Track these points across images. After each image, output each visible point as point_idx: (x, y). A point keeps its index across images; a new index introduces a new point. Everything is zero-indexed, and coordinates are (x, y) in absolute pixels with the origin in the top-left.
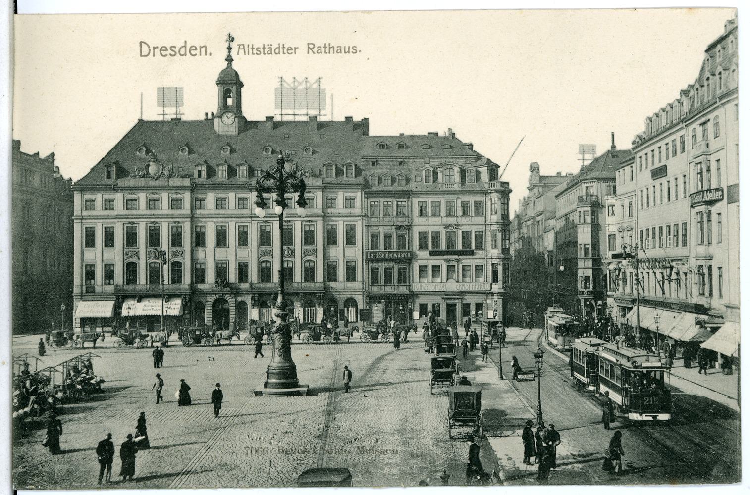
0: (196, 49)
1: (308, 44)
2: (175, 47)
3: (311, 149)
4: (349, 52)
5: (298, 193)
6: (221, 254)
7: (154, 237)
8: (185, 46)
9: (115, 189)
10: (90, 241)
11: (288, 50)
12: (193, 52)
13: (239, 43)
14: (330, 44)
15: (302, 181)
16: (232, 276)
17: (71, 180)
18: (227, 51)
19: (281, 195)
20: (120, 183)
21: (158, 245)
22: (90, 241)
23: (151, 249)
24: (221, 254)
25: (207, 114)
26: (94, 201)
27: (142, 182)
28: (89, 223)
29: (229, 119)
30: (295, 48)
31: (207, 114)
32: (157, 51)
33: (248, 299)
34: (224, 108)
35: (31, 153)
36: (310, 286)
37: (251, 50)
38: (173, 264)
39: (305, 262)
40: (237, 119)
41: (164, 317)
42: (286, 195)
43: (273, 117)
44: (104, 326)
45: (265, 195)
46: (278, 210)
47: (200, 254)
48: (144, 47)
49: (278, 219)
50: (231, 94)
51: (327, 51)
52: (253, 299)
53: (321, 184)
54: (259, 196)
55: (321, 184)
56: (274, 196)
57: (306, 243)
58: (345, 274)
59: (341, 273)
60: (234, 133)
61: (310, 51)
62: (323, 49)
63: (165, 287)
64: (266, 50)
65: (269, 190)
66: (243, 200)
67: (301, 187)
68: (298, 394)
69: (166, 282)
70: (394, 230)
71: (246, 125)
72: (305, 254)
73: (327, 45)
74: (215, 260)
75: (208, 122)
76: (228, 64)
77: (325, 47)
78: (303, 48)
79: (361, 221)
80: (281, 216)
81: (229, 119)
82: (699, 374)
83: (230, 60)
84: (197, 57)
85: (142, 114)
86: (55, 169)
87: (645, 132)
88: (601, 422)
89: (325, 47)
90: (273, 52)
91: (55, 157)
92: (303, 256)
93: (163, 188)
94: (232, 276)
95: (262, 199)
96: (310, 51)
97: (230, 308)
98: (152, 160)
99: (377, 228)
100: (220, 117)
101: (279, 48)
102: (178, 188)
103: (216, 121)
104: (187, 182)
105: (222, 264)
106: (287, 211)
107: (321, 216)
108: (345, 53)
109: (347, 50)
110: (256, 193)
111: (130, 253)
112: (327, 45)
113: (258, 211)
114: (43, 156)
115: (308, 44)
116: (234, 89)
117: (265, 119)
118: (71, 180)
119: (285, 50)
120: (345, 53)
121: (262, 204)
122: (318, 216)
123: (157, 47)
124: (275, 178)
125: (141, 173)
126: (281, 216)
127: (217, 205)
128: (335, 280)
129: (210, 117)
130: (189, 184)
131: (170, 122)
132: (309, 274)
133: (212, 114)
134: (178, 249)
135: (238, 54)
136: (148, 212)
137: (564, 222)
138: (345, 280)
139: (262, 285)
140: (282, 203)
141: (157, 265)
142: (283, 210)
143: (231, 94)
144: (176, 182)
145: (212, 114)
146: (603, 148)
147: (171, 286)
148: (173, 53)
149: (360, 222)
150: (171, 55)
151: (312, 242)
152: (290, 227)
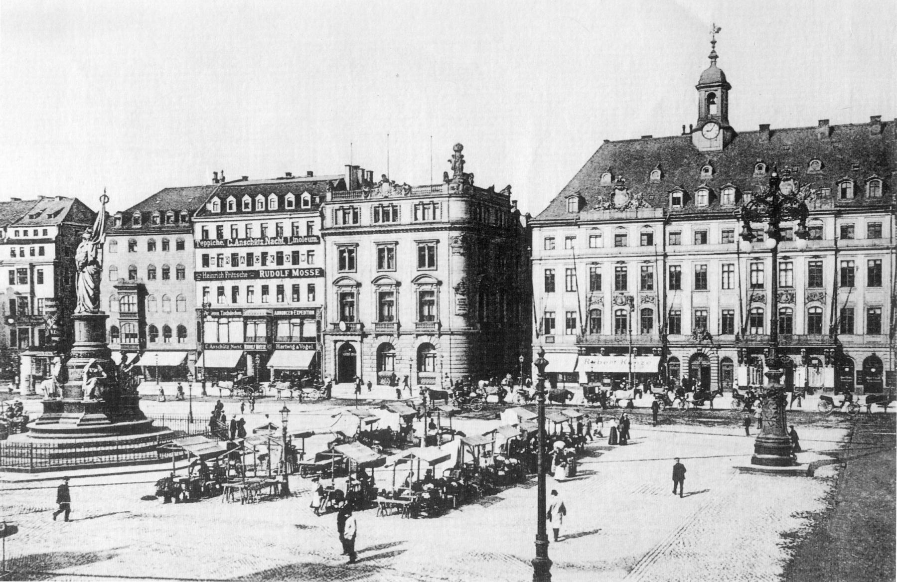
5: (798, 221)
7: (621, 282)
9: (576, 223)
10: (550, 286)
15: (803, 206)
18: (711, 45)
19: (774, 223)
20: (584, 216)
21: (626, 289)
22: (550, 286)
23: (617, 293)
24: (700, 298)
25: (684, 127)
26: (680, 234)
27: (607, 215)
28: (550, 265)
29: (712, 130)
31: (684, 127)
33: (733, 354)
34: (705, 119)
35: (486, 187)
36: (815, 340)
38: (643, 311)
39: (809, 309)
40: (721, 130)
41: (632, 374)
42: (782, 225)
43: (769, 125)
44: (566, 381)
45: (754, 225)
46: (770, 243)
49: (771, 254)
50: (715, 100)
52: (740, 354)
53: (833, 208)
54: (747, 226)
55: (833, 208)
56: (765, 225)
57: (811, 284)
59: (860, 323)
60: (718, 149)
63: (634, 338)
65: (758, 218)
66: (728, 232)
67: (801, 213)
68: (794, 473)
69: (634, 333)
71: (731, 136)
72: (810, 298)
75: (687, 137)
76: (712, 62)
80: (774, 251)
81: (712, 130)
82: (673, 494)
83: (714, 57)
86: (511, 204)
91: (512, 190)
93: (630, 221)
95: (750, 229)
97: (712, 365)
98: (619, 187)
100: (700, 129)
102: (647, 221)
103: (696, 136)
104: (659, 213)
105: (729, 311)
106: (782, 245)
110: (742, 223)
113: (745, 246)
114: (497, 190)
116: (718, 93)
117: (758, 128)
121: (749, 236)
124: (766, 203)
125: (606, 205)
126: (774, 251)
127: (696, 240)
128: (850, 331)
129: (688, 130)
130: (661, 216)
131: (640, 140)
132: (814, 322)
133: (691, 126)
134: (817, 290)
136: (870, 242)
139: (811, 337)
140: (776, 234)
141: (624, 313)
142: (778, 243)
143: (715, 100)
144: (646, 213)
145: (691, 126)
151: (820, 285)
152: (819, 264)
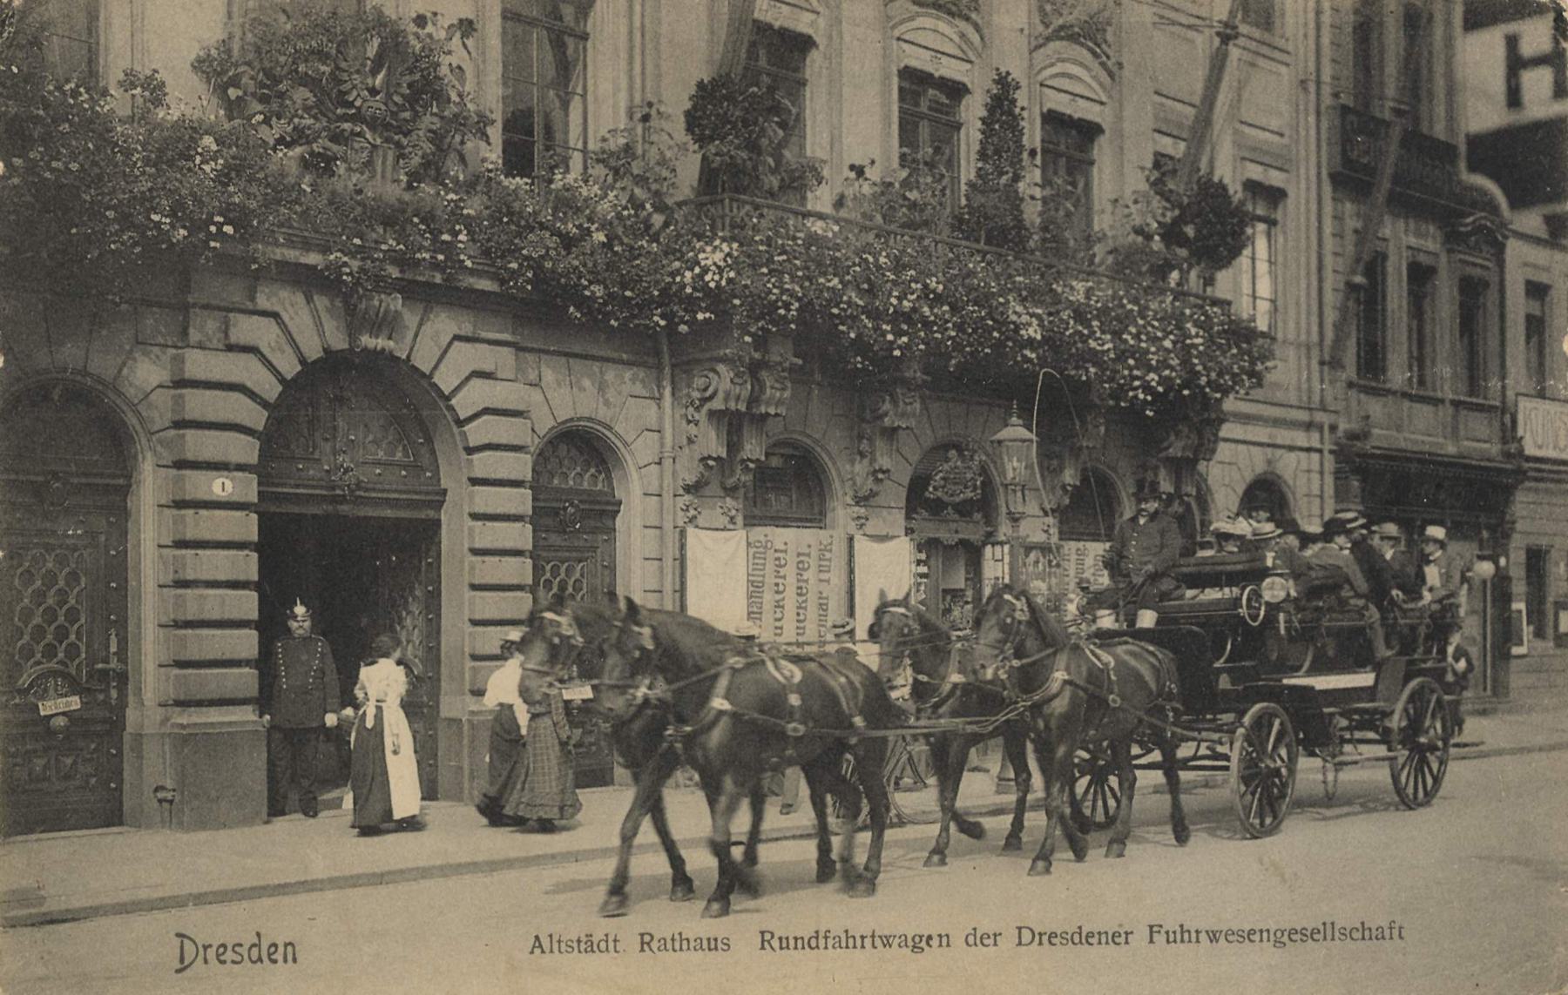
0: (1319, 932)
1: (642, 935)
2: (241, 945)
4: (716, 948)
8: (1080, 934)
11: (1087, 936)
12: (986, 942)
13: (643, 931)
14: (680, 934)
17: (1080, 855)
30: (995, 935)
32: (1045, 938)
37: (556, 946)
51: (677, 946)
61: (646, 947)
64: (583, 946)
85: (436, 367)
87: (340, 400)
88: (809, 836)
90: (595, 948)
96: (646, 947)
101: (817, 938)
108: (710, 949)
109: (1265, 934)
112: (677, 937)
115: (642, 935)
118: (1080, 855)
119: (563, 945)
120: (1268, 931)
123: (210, 946)
137: (937, 832)
148: (238, 958)
150: (234, 962)
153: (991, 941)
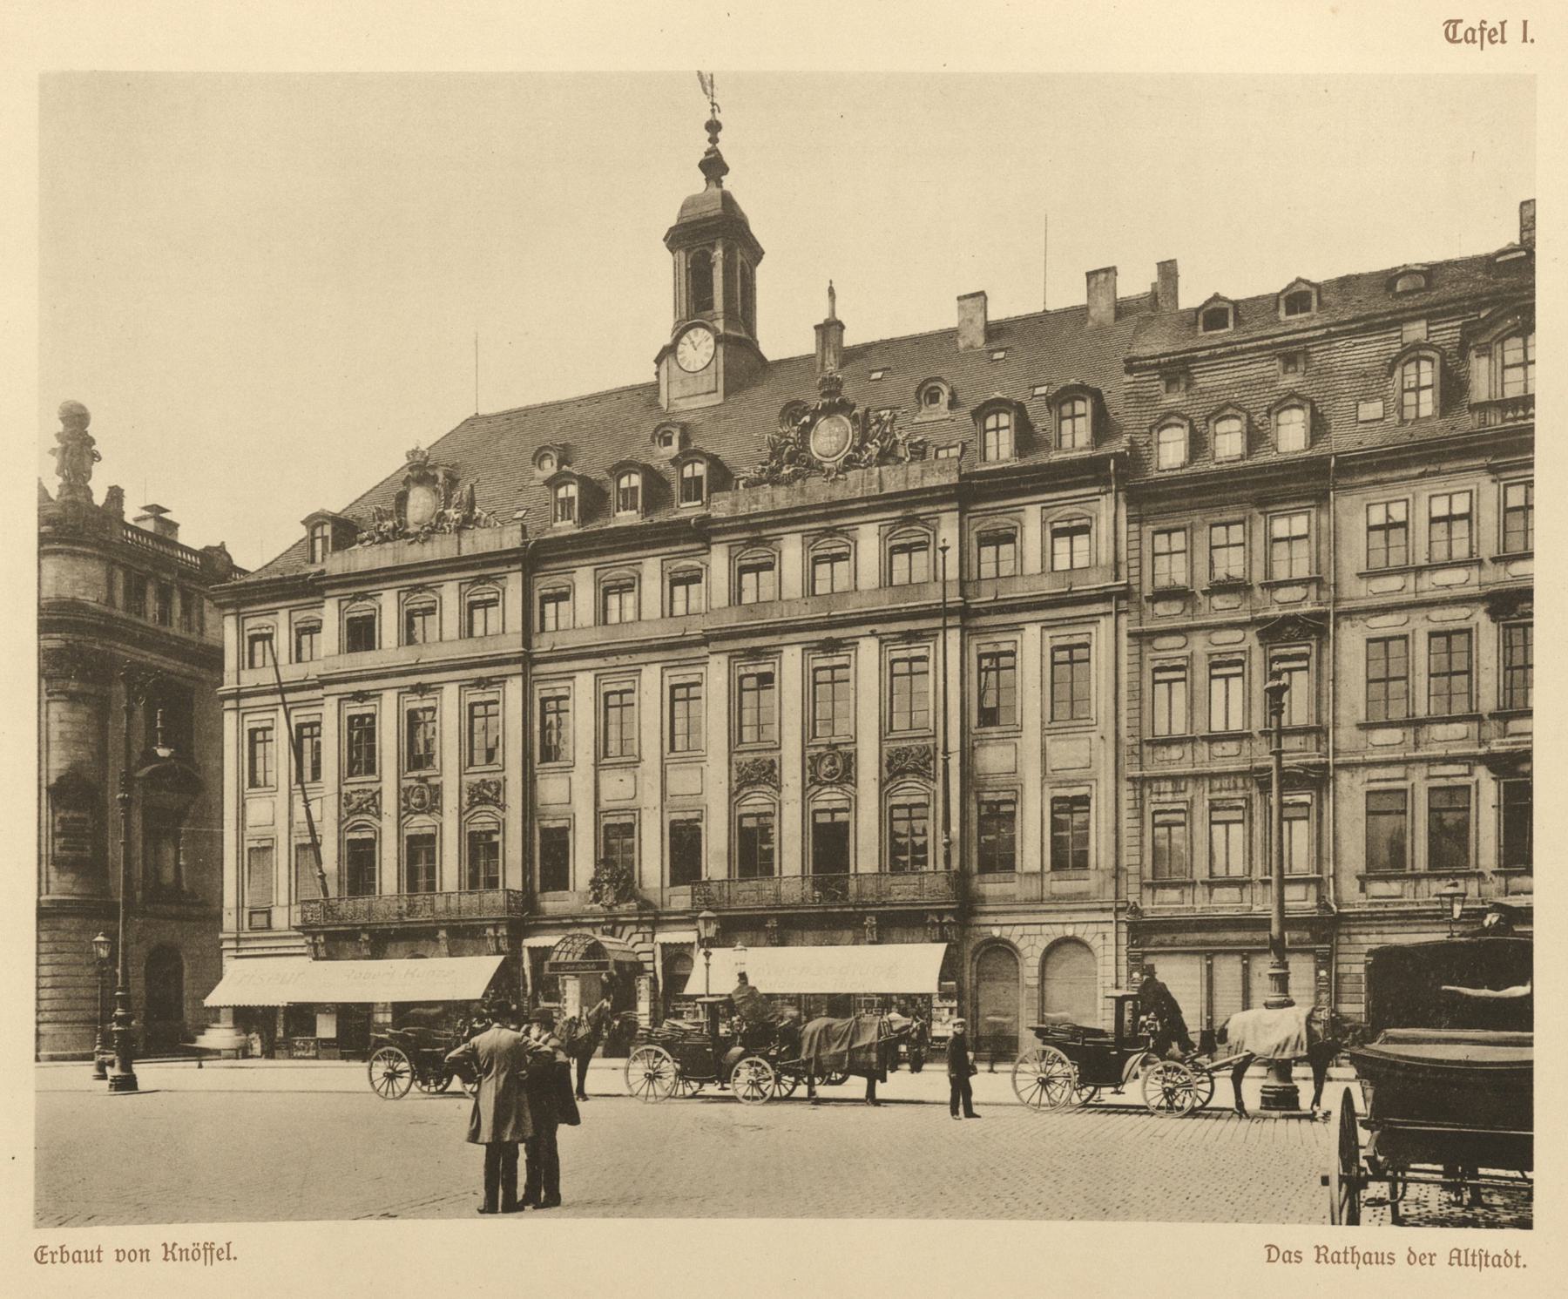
3: (946, 390)
6: (616, 787)
16: (652, 863)
24: (616, 787)
47: (993, 758)
48: (1274, 1251)
58: (571, 865)
62: (1342, 1256)
70: (1255, 643)
73: (1349, 1250)
74: (597, 804)
77: (1345, 1253)
78: (1401, 1257)
79: (1111, 620)
84: (1499, 44)
89: (1345, 1253)
92: (886, 775)
94: (652, 863)
99: (1178, 641)
107: (516, 661)
111: (355, 797)
112: (1349, 1250)
119: (1486, 33)
122: (507, 662)
135: (1525, 23)
138: (667, 883)
146: (1135, 283)
147: (466, 900)
149: (1106, 624)
153: (1427, 1261)
